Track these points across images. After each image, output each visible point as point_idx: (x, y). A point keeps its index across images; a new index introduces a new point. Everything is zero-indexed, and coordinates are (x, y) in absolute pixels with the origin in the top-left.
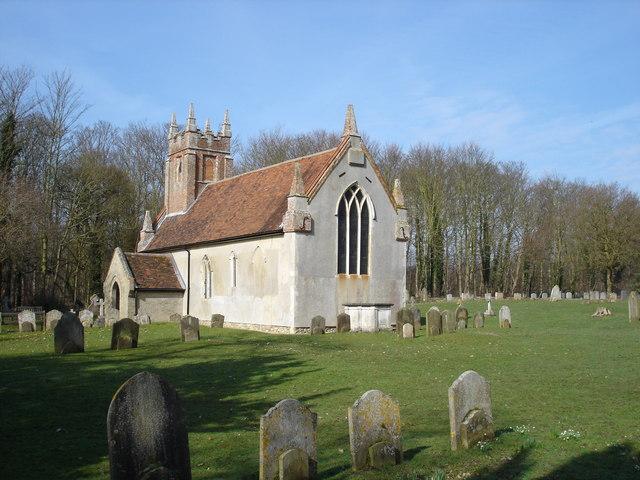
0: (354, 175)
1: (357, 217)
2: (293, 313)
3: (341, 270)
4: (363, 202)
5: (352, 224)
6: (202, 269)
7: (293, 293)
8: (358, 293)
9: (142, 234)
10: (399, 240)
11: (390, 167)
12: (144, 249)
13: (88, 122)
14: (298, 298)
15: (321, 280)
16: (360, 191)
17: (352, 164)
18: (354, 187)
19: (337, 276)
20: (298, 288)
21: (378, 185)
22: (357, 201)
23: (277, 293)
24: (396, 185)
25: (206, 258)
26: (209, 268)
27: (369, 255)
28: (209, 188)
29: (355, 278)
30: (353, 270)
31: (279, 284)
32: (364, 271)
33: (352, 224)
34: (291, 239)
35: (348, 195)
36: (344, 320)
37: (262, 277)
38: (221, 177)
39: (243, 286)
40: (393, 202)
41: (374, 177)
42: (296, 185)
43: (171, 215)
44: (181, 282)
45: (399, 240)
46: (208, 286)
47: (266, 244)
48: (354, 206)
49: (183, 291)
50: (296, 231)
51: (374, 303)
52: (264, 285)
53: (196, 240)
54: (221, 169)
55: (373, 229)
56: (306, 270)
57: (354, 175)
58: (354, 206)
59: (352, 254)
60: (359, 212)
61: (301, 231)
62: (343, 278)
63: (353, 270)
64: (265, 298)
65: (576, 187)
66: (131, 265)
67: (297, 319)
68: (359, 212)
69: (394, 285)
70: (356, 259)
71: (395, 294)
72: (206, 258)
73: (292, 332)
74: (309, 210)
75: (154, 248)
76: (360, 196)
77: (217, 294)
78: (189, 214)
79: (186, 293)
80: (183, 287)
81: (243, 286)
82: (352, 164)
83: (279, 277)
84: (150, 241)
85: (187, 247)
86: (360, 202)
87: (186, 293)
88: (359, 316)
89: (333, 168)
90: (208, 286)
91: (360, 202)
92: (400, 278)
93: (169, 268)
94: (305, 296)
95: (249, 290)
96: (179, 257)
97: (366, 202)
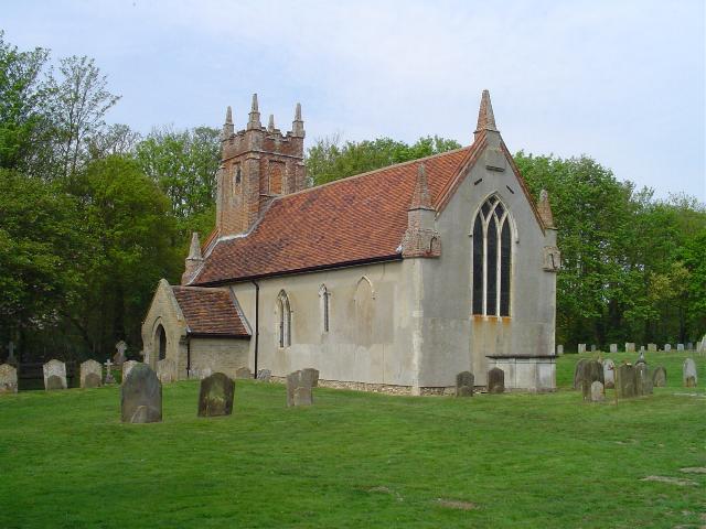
0: (493, 184)
1: (496, 239)
2: (417, 368)
3: (477, 310)
4: (503, 219)
5: (491, 250)
6: (277, 309)
7: (416, 340)
8: (498, 341)
9: (188, 264)
10: (547, 271)
11: (535, 177)
12: (191, 281)
13: (114, 117)
14: (423, 348)
15: (452, 323)
16: (499, 206)
17: (490, 169)
18: (492, 200)
19: (472, 317)
20: (424, 334)
21: (521, 198)
22: (483, 217)
23: (392, 342)
24: (541, 199)
25: (283, 293)
26: (286, 306)
27: (511, 290)
28: (277, 203)
29: (494, 320)
30: (491, 311)
31: (396, 328)
32: (505, 312)
33: (491, 250)
34: (414, 270)
35: (485, 208)
36: (497, 378)
37: (368, 319)
38: (293, 189)
39: (338, 331)
40: (539, 220)
41: (517, 187)
42: (421, 195)
43: (224, 239)
44: (246, 325)
45: (547, 271)
46: (285, 331)
47: (374, 277)
48: (492, 225)
49: (248, 338)
50: (422, 257)
51: (535, 354)
52: (371, 329)
53: (270, 270)
54: (292, 178)
55: (516, 255)
56: (434, 312)
57: (493, 184)
58: (492, 225)
59: (491, 290)
60: (485, 230)
61: (428, 256)
62: (478, 321)
63: (491, 311)
64: (374, 347)
65: (530, 168)
66: (182, 298)
67: (422, 376)
68: (485, 230)
69: (541, 329)
70: (501, 302)
71: (542, 343)
72: (283, 293)
73: (416, 392)
74: (438, 228)
75: (205, 281)
76: (500, 210)
77: (300, 341)
78: (252, 236)
79: (254, 338)
80: (249, 332)
81: (338, 331)
82: (490, 169)
83: (396, 319)
84: (198, 272)
85: (255, 280)
86: (500, 218)
87: (254, 338)
88: (512, 372)
89: (467, 172)
90: (285, 331)
91: (500, 218)
92: (547, 321)
93: (230, 309)
94: (434, 347)
95: (358, 340)
96: (244, 297)
97: (507, 219)
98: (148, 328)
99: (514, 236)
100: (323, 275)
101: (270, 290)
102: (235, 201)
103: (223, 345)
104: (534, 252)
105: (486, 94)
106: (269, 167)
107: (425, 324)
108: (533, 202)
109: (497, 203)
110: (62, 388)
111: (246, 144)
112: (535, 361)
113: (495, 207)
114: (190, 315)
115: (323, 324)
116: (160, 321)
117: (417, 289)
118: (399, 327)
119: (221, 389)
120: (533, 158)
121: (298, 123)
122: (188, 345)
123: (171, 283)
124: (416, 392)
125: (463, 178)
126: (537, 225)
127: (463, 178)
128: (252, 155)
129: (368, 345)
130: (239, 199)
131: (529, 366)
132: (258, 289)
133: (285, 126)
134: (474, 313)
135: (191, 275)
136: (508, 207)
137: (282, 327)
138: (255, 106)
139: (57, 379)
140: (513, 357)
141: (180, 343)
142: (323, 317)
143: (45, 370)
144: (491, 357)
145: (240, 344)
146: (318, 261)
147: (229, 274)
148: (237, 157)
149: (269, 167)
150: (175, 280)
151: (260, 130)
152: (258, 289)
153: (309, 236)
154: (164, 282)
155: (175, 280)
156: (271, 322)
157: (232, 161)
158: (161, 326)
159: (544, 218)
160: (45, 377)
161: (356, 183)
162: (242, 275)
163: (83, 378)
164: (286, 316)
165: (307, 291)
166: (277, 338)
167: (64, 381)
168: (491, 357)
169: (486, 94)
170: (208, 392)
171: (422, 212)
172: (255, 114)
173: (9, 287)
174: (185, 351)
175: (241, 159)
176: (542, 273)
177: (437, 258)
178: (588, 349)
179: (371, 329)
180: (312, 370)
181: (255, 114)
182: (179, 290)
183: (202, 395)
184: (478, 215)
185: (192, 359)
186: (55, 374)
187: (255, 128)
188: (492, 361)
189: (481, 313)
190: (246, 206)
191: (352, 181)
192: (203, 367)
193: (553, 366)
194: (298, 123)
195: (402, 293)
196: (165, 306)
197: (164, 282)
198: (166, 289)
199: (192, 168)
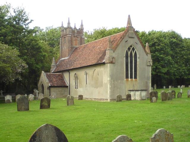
0: (131, 42)
2: (109, 94)
4: (134, 52)
5: (131, 61)
7: (109, 86)
8: (133, 86)
10: (148, 66)
12: (53, 71)
14: (111, 88)
15: (119, 81)
18: (131, 46)
19: (125, 79)
20: (111, 84)
31: (104, 83)
32: (136, 78)
33: (131, 61)
35: (129, 49)
37: (97, 80)
40: (145, 51)
43: (62, 59)
44: (67, 83)
47: (98, 69)
48: (131, 54)
49: (67, 87)
52: (98, 84)
53: (72, 68)
56: (114, 78)
58: (131, 54)
59: (131, 71)
61: (112, 63)
62: (127, 80)
63: (131, 77)
64: (98, 88)
66: (49, 77)
67: (111, 96)
71: (147, 86)
74: (114, 55)
76: (133, 49)
77: (80, 87)
79: (69, 87)
80: (67, 85)
84: (54, 69)
85: (69, 71)
86: (133, 52)
87: (69, 87)
88: (135, 95)
93: (62, 79)
96: (66, 75)
97: (135, 52)
98: (39, 84)
99: (138, 56)
100: (85, 69)
101: (72, 74)
102: (65, 48)
103: (60, 89)
104: (144, 62)
105: (129, 16)
106: (74, 39)
107: (111, 82)
108: (144, 47)
109: (132, 47)
110: (11, 103)
111: (67, 32)
112: (140, 91)
113: (132, 48)
114: (50, 81)
115: (85, 82)
116: (42, 83)
117: (109, 71)
118: (105, 83)
119: (47, 101)
120: (93, 33)
121: (82, 25)
122: (50, 89)
123: (45, 72)
124: (109, 101)
125: (122, 40)
126: (145, 53)
127: (122, 40)
128: (68, 35)
129: (97, 88)
130: (66, 48)
131: (138, 93)
132: (69, 73)
133: (78, 27)
134: (126, 78)
135: (53, 70)
136: (136, 48)
137: (76, 83)
138: (82, 23)
139: (9, 100)
140: (136, 91)
141: (47, 89)
142: (85, 79)
143: (5, 98)
144: (129, 91)
145: (65, 89)
146: (84, 65)
147: (62, 69)
148: (64, 36)
149: (74, 39)
150: (47, 70)
151: (71, 28)
152: (69, 73)
153: (83, 58)
154: (43, 72)
155: (47, 70)
156: (73, 83)
157: (63, 37)
158: (42, 84)
159: (147, 51)
160: (6, 100)
161: (96, 42)
162: (65, 69)
163: (17, 100)
164: (77, 81)
165: (81, 74)
166: (74, 87)
167: (11, 101)
168: (129, 91)
169: (129, 16)
170: (43, 102)
171: (108, 51)
172: (69, 23)
173: (173, 62)
174: (49, 91)
175: (66, 36)
176: (146, 66)
177: (114, 63)
178: (172, 87)
179: (98, 84)
180: (81, 95)
181: (69, 23)
182: (47, 74)
183: (41, 103)
184: (127, 51)
185: (51, 93)
186: (8, 99)
187: (69, 28)
188: (129, 92)
189: (128, 78)
190: (67, 50)
191: (95, 42)
192: (52, 95)
193: (146, 93)
194: (82, 25)
195: (104, 74)
196: (43, 77)
197: (43, 72)
198: (43, 74)
199: (55, 38)
